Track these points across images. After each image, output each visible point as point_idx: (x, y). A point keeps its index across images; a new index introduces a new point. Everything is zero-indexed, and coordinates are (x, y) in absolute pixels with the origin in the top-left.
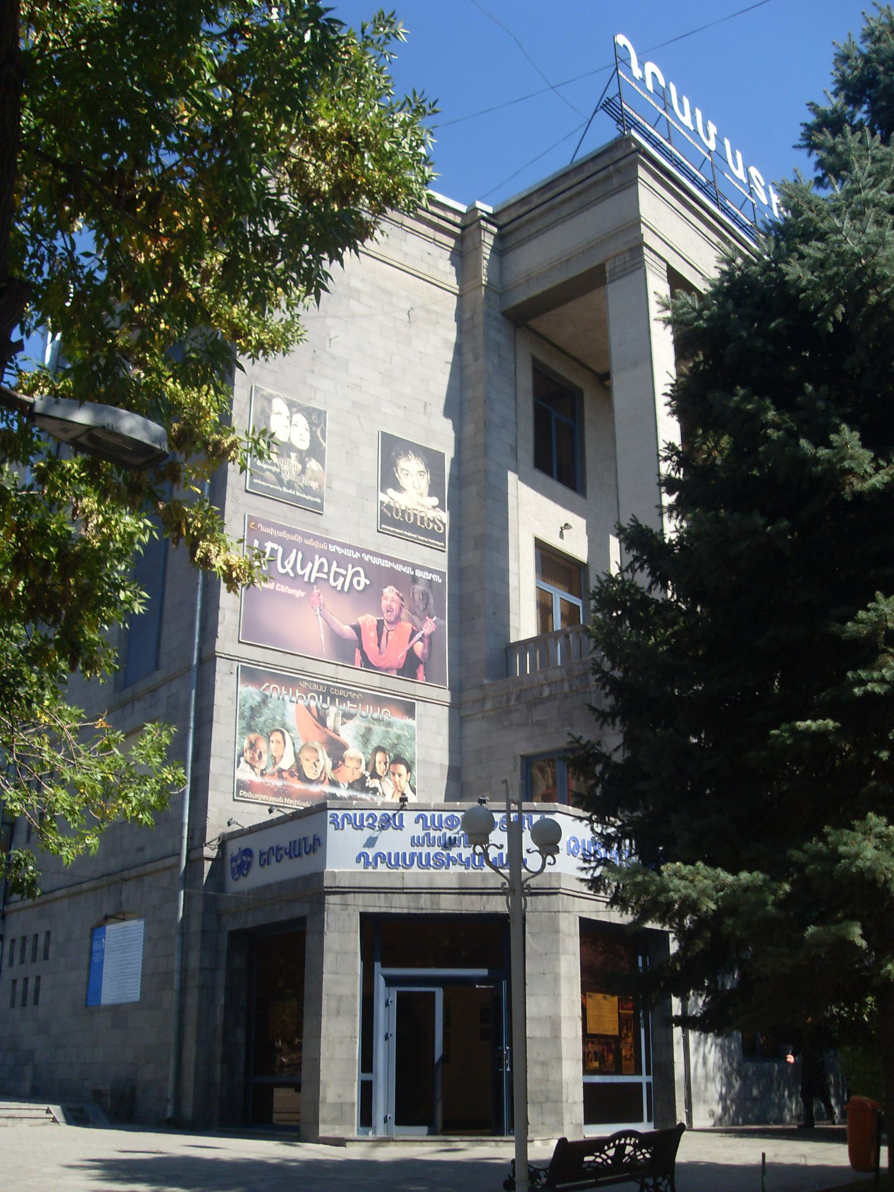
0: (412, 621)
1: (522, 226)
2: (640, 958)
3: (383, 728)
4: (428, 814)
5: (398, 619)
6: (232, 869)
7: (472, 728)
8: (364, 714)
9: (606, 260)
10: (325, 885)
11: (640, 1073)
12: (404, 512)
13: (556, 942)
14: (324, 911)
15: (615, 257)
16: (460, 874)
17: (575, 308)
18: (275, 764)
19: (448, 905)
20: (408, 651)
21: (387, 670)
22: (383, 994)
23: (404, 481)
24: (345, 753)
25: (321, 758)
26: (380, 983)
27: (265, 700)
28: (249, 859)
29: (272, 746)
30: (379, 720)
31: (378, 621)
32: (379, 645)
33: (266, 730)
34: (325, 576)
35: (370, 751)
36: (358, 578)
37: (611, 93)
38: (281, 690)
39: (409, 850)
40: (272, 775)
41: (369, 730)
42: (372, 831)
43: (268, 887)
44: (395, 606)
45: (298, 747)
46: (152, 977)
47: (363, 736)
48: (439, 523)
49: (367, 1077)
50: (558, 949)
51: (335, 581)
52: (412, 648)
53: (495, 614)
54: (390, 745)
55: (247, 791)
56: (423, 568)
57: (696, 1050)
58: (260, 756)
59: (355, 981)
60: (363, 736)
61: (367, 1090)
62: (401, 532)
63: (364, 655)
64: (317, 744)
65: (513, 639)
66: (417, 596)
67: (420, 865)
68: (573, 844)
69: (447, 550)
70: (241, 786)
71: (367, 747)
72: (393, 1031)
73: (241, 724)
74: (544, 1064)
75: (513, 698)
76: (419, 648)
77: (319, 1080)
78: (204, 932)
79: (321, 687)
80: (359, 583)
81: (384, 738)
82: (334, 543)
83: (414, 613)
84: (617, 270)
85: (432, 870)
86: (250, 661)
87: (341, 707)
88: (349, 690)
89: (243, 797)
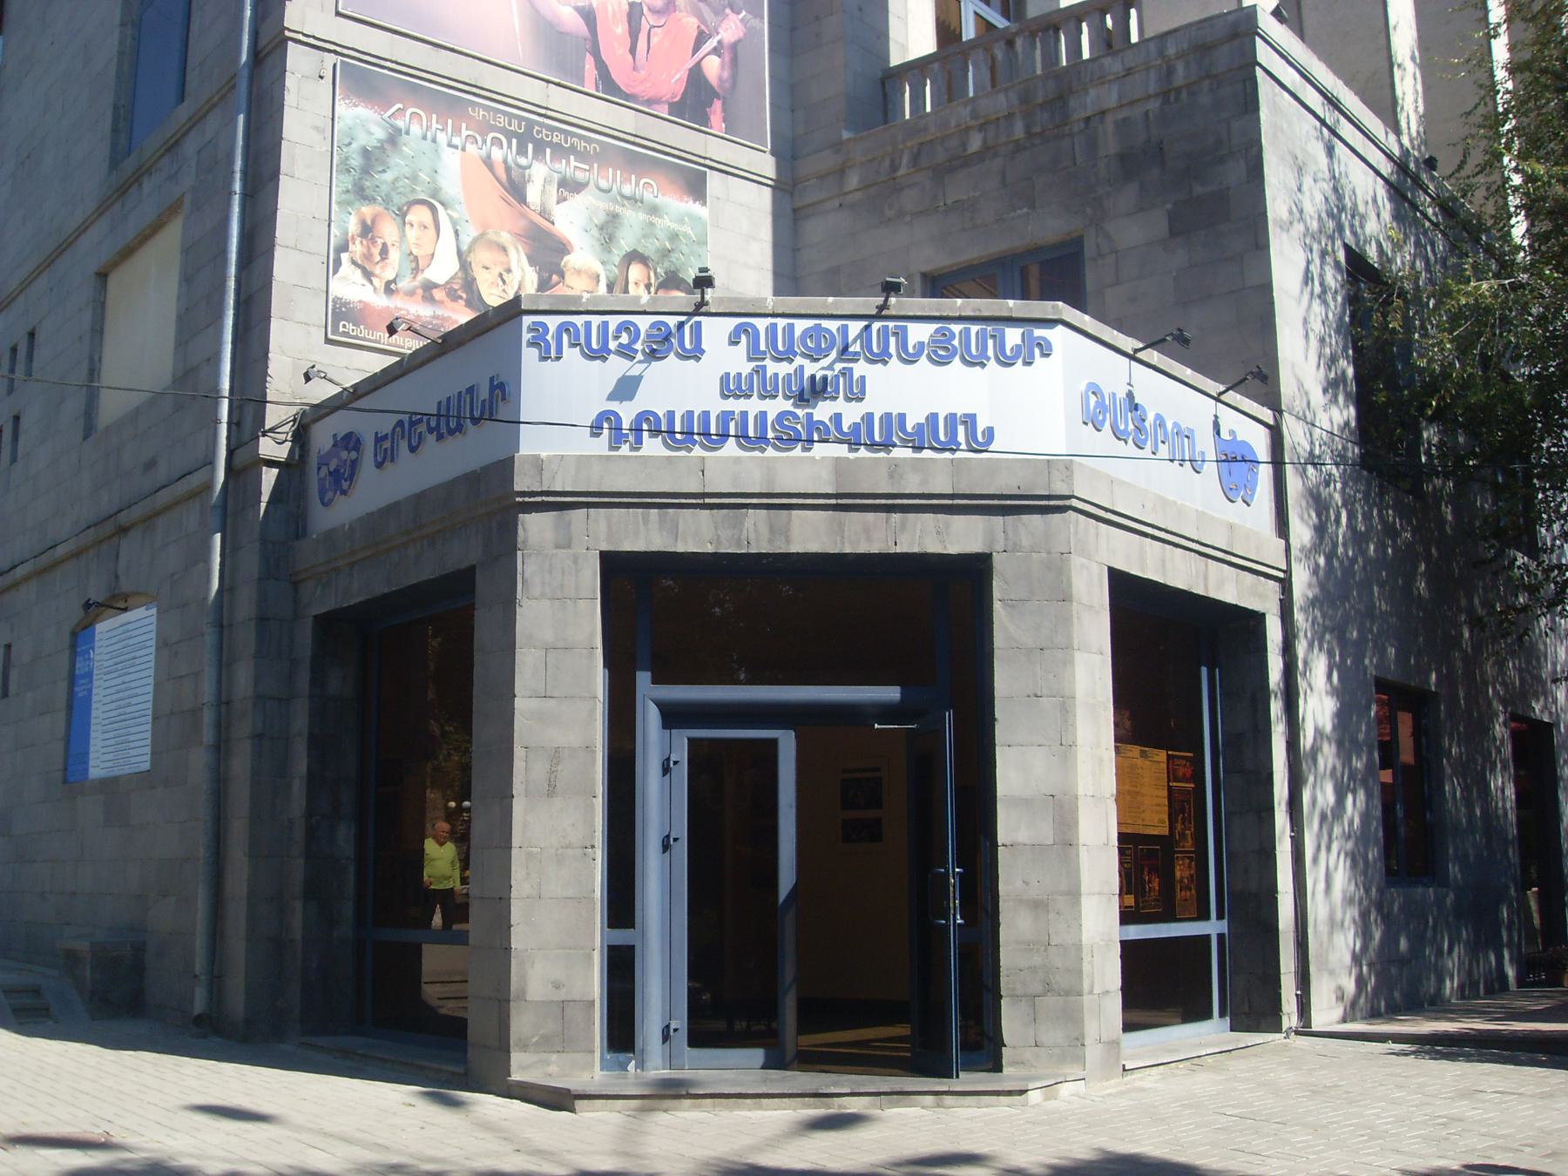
0: (699, 15)
2: (1204, 670)
3: (642, 216)
4: (761, 324)
6: (321, 481)
7: (816, 229)
8: (604, 184)
10: (517, 488)
11: (1206, 917)
13: (1067, 620)
14: (514, 549)
16: (838, 459)
18: (416, 270)
19: (810, 535)
22: (657, 744)
24: (566, 258)
25: (514, 267)
26: (649, 720)
27: (394, 138)
28: (354, 455)
29: (411, 234)
30: (633, 200)
32: (633, 51)
33: (398, 200)
35: (617, 260)
38: (429, 120)
39: (717, 406)
40: (411, 293)
41: (614, 218)
43: (393, 509)
45: (466, 240)
46: (170, 719)
49: (622, 937)
50: (1070, 637)
52: (698, 64)
54: (657, 250)
55: (356, 324)
57: (1315, 860)
58: (384, 252)
59: (592, 712)
61: (621, 968)
63: (602, 67)
64: (505, 238)
65: (895, 61)
67: (742, 436)
68: (1093, 399)
70: (341, 312)
71: (610, 252)
72: (681, 830)
73: (343, 182)
74: (1038, 906)
75: (905, 160)
76: (713, 67)
77: (508, 949)
78: (262, 620)
79: (515, 122)
81: (645, 236)
85: (770, 452)
86: (362, 55)
87: (557, 166)
88: (574, 135)
89: (346, 334)
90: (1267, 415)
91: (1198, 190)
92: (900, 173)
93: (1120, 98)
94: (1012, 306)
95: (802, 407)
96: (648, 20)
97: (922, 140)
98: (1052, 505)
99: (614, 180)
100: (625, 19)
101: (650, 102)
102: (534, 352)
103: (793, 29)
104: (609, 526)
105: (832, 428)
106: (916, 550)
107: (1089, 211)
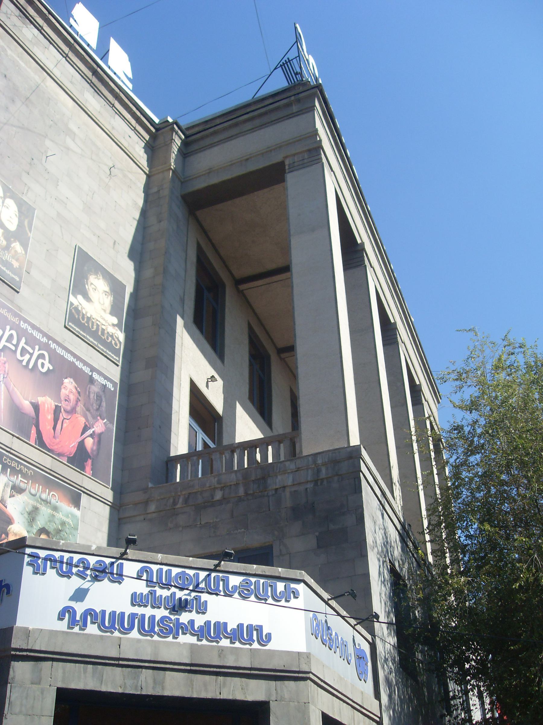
1: (207, 136)
3: (49, 511)
5: (73, 411)
8: (33, 491)
9: (286, 157)
10: (13, 646)
12: (89, 319)
14: (6, 682)
15: (294, 155)
16: (192, 645)
17: (239, 206)
19: (175, 686)
20: (79, 443)
21: (59, 455)
23: (92, 294)
24: (10, 527)
31: (56, 406)
32: (54, 428)
34: (13, 348)
35: (35, 531)
36: (43, 361)
37: (292, 54)
39: (129, 610)
42: (82, 581)
44: (72, 397)
47: (29, 514)
48: (116, 340)
51: (22, 355)
53: (160, 427)
54: (55, 529)
56: (100, 373)
60: (29, 514)
62: (85, 334)
63: (39, 433)
65: (172, 454)
66: (92, 396)
69: (120, 364)
71: (32, 526)
75: (181, 500)
76: (89, 443)
80: (43, 365)
81: (50, 521)
82: (26, 321)
83: (88, 410)
84: (296, 164)
87: (12, 478)
88: (22, 464)
90: (369, 637)
91: (332, 527)
92: (178, 506)
93: (293, 480)
94: (281, 571)
95: (174, 615)
96: (63, 415)
97: (190, 492)
98: (299, 676)
99: (38, 490)
100: (52, 412)
101: (59, 455)
102: (31, 569)
103: (126, 432)
104: (64, 673)
105: (189, 628)
106: (230, 697)
107: (276, 533)
